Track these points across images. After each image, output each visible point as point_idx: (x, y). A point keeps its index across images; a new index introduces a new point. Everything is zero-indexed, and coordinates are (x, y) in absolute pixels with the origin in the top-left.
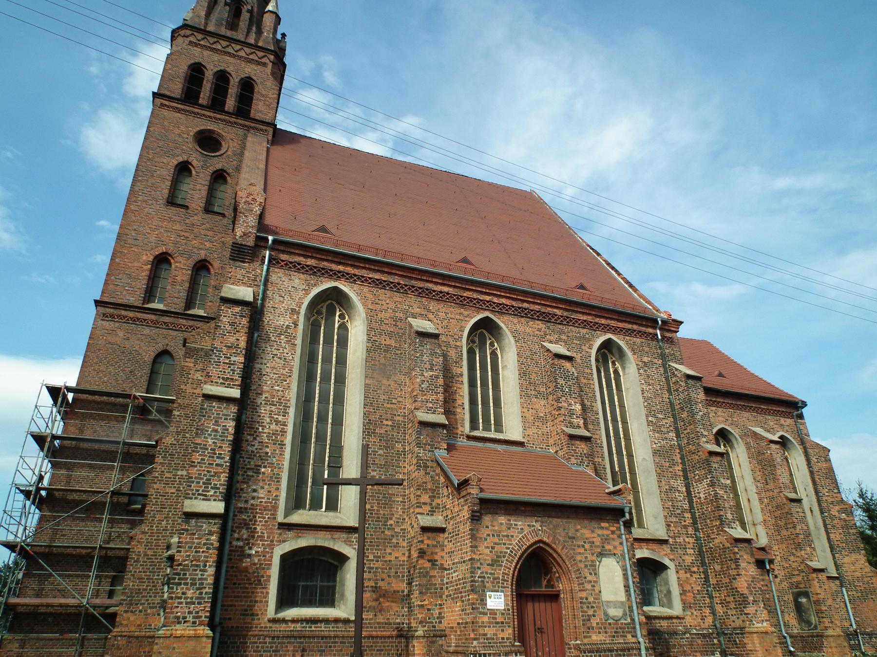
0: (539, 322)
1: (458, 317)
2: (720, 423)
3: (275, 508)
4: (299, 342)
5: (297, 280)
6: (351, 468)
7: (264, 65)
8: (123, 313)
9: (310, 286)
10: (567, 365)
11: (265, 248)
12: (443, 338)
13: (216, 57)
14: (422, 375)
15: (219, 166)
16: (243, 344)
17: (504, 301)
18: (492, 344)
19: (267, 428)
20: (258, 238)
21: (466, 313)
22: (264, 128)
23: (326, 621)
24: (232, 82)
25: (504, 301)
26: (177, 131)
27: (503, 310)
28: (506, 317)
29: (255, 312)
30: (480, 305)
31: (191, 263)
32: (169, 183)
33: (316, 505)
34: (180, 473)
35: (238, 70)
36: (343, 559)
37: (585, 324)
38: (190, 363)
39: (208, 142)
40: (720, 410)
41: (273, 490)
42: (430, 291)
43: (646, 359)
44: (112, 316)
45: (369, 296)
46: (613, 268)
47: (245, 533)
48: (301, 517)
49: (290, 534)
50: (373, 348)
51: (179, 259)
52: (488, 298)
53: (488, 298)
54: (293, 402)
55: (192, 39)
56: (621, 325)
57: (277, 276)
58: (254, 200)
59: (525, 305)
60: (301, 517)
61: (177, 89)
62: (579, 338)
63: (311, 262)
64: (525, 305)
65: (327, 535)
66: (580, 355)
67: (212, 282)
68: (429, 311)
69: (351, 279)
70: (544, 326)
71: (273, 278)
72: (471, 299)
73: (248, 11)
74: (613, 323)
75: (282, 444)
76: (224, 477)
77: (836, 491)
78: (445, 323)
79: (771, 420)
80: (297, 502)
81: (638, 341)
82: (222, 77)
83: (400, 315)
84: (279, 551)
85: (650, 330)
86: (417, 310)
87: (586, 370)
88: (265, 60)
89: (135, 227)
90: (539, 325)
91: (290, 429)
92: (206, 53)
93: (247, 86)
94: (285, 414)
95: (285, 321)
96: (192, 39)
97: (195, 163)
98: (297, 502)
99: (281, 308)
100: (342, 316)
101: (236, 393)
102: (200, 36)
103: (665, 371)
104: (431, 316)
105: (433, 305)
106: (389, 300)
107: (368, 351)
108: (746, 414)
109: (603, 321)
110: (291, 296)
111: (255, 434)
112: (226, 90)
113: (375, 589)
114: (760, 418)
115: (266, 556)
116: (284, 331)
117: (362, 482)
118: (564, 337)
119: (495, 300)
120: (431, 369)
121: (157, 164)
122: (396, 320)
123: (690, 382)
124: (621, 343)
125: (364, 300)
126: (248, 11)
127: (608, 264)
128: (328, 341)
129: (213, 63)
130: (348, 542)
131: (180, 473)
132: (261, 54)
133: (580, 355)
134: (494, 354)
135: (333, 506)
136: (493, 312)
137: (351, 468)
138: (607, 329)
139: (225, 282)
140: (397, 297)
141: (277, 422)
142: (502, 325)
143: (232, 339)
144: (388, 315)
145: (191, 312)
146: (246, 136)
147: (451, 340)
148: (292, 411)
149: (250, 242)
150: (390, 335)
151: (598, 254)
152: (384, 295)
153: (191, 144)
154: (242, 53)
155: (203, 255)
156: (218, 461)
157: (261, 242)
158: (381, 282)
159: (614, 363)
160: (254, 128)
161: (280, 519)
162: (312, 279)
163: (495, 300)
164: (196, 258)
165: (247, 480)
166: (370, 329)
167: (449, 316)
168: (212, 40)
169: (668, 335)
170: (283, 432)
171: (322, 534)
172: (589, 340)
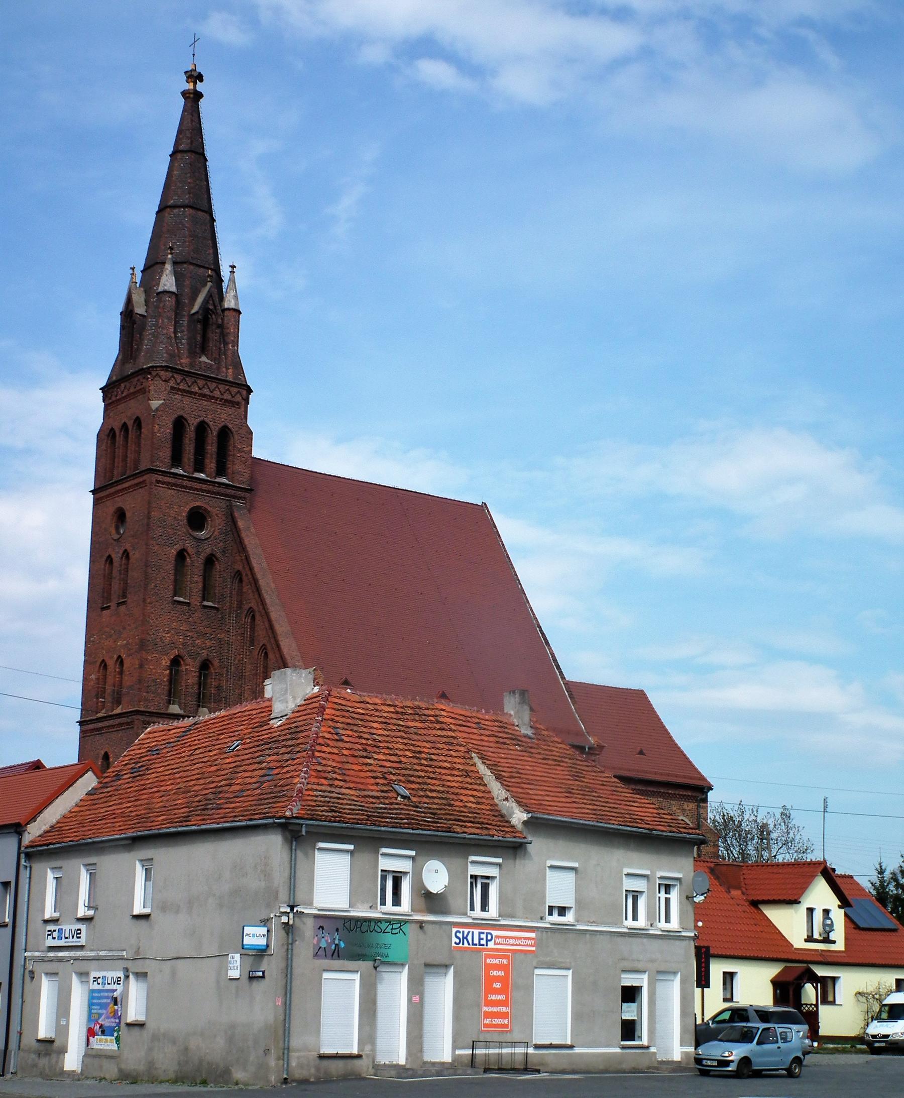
15: (208, 551)
31: (197, 663)
32: (172, 577)
51: (189, 661)
55: (172, 383)
82: (202, 428)
92: (187, 400)
93: (224, 434)
96: (172, 383)
97: (190, 550)
102: (179, 378)
154: (217, 394)
155: (204, 654)
160: (235, 497)
169: (593, 758)
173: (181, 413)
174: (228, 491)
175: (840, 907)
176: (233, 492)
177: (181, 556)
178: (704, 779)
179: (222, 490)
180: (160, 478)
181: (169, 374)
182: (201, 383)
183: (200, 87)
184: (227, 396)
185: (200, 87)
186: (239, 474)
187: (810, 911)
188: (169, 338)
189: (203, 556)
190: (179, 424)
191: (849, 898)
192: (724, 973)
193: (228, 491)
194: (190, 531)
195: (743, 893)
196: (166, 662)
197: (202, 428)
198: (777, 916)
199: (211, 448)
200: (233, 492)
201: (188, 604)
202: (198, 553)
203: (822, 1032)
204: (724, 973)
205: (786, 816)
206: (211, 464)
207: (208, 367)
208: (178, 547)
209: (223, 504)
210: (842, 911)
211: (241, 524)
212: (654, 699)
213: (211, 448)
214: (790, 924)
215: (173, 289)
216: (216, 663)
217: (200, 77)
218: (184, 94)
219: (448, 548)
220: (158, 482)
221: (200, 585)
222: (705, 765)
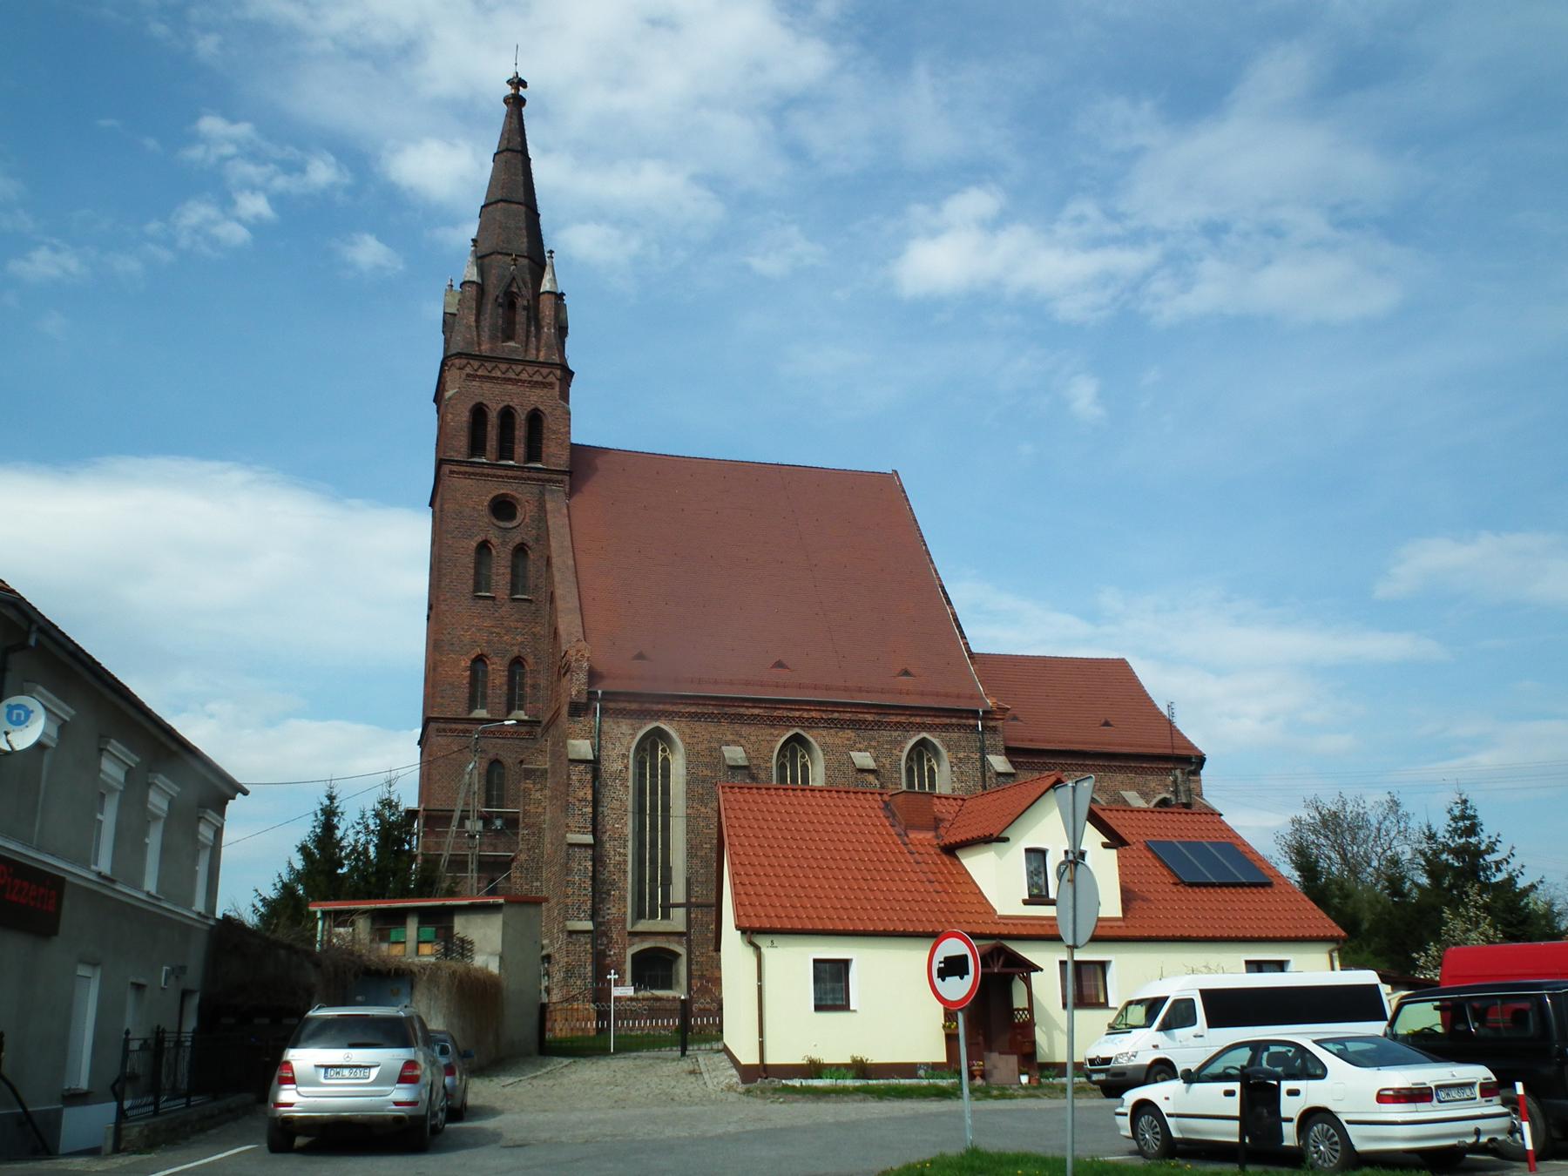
3: (625, 920)
4: (630, 784)
5: (624, 727)
6: (678, 893)
7: (551, 385)
8: (454, 726)
9: (636, 730)
10: (871, 778)
11: (596, 699)
13: (498, 389)
15: (518, 540)
16: (590, 797)
17: (813, 714)
18: (803, 757)
19: (613, 860)
20: (589, 693)
22: (560, 477)
23: (668, 1000)
24: (518, 421)
25: (813, 714)
27: (812, 724)
28: (815, 732)
29: (594, 765)
30: (788, 722)
31: (506, 661)
32: (472, 572)
33: (653, 916)
35: (524, 400)
36: (677, 955)
37: (898, 725)
38: (529, 784)
39: (503, 508)
41: (622, 906)
42: (742, 715)
43: (961, 755)
45: (687, 731)
46: (959, 626)
47: (605, 940)
48: (644, 925)
49: (636, 939)
50: (692, 781)
51: (496, 659)
52: (797, 714)
53: (797, 714)
54: (630, 836)
55: (468, 370)
56: (937, 721)
57: (609, 725)
59: (836, 715)
60: (644, 925)
61: (462, 443)
63: (634, 706)
64: (836, 715)
67: (529, 681)
71: (605, 727)
72: (781, 718)
73: (525, 308)
74: (928, 720)
75: (625, 872)
76: (589, 903)
79: (1153, 782)
80: (639, 915)
81: (955, 735)
82: (507, 414)
83: (715, 745)
84: (630, 952)
85: (972, 722)
86: (730, 737)
88: (551, 379)
90: (850, 734)
91: (630, 859)
92: (487, 385)
93: (535, 418)
94: (625, 847)
95: (618, 766)
96: (468, 370)
97: (494, 540)
98: (639, 915)
99: (614, 754)
100: (664, 750)
101: (589, 839)
102: (476, 364)
103: (983, 766)
104: (743, 741)
105: (745, 730)
106: (704, 730)
107: (688, 783)
108: (1120, 777)
109: (918, 720)
110: (624, 739)
111: (604, 866)
112: (513, 429)
113: (702, 977)
114: (1139, 779)
115: (622, 954)
116: (619, 775)
117: (688, 905)
119: (805, 715)
122: (711, 750)
123: (1002, 779)
124: (935, 741)
125: (682, 734)
126: (525, 308)
127: (956, 620)
128: (654, 776)
129: (495, 397)
130: (680, 943)
132: (545, 371)
134: (805, 767)
135: (666, 916)
136: (802, 727)
137: (678, 893)
139: (567, 737)
143: (581, 794)
146: (542, 494)
148: (630, 844)
149: (584, 700)
150: (707, 765)
151: (949, 602)
153: (486, 518)
154: (524, 376)
155: (516, 651)
157: (592, 696)
158: (696, 714)
159: (929, 760)
160: (549, 481)
161: (629, 928)
162: (636, 723)
163: (805, 715)
164: (509, 657)
165: (602, 901)
166: (689, 762)
168: (489, 365)
169: (992, 724)
170: (625, 862)
173: (480, 399)
174: (541, 476)
175: (1105, 846)
176: (547, 476)
177: (484, 547)
178: (1192, 747)
179: (535, 475)
180: (455, 468)
181: (464, 361)
182: (503, 367)
183: (522, 91)
184: (537, 378)
185: (522, 91)
186: (555, 456)
187: (1036, 855)
188: (469, 327)
189: (510, 547)
190: (479, 412)
191: (1122, 831)
192: (816, 961)
193: (541, 476)
194: (502, 524)
195: (937, 837)
196: (465, 662)
197: (507, 414)
198: (982, 866)
199: (520, 433)
200: (547, 476)
201: (493, 598)
202: (504, 543)
203: (941, 1056)
204: (816, 961)
205: (1394, 805)
206: (520, 449)
207: (515, 350)
208: (479, 539)
209: (536, 490)
210: (1113, 853)
211: (548, 506)
212: (1149, 676)
213: (520, 433)
214: (998, 878)
215: (475, 278)
216: (530, 659)
217: (523, 83)
218: (506, 100)
219: (859, 527)
220: (452, 472)
221: (508, 577)
222: (1196, 735)
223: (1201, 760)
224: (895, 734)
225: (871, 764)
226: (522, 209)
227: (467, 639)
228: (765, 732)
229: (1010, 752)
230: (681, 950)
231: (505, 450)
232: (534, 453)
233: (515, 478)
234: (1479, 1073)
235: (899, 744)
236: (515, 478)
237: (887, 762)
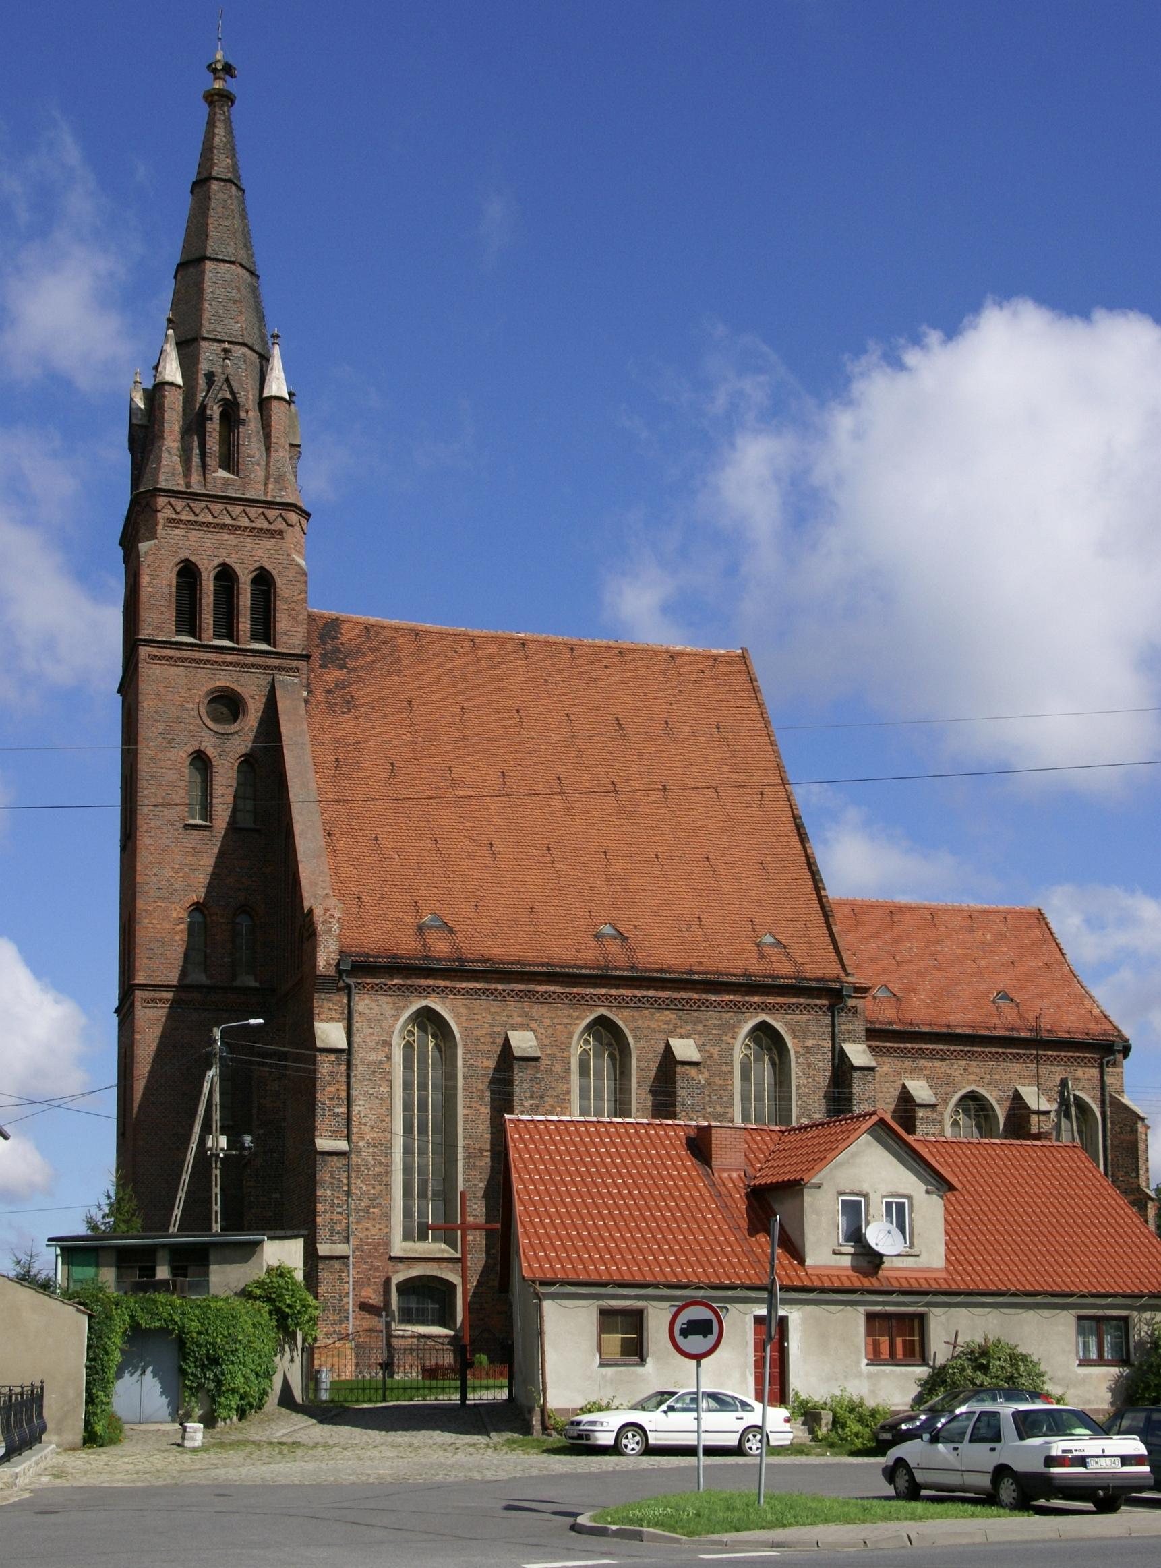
0: (667, 1012)
1: (566, 1021)
2: (970, 1083)
12: (545, 1062)
14: (522, 1105)
21: (576, 1014)
22: (294, 664)
26: (178, 700)
28: (626, 1012)
34: (274, 1196)
35: (246, 557)
37: (729, 1006)
39: (227, 704)
40: (974, 1064)
43: (809, 1043)
44: (153, 1000)
45: (463, 1011)
49: (401, 1266)
58: (332, 916)
62: (720, 1027)
65: (433, 1265)
66: (718, 1048)
68: (532, 1018)
69: (441, 992)
70: (673, 1016)
77: (1134, 1175)
78: (550, 1032)
82: (226, 575)
87: (724, 1068)
89: (155, 871)
90: (670, 1015)
93: (264, 581)
104: (533, 1025)
105: (537, 1011)
108: (1018, 1067)
118: (700, 1028)
120: (532, 1097)
121: (162, 764)
124: (778, 1026)
125: (457, 1016)
130: (453, 1271)
131: (274, 1196)
133: (718, 1048)
138: (763, 1007)
140: (495, 1006)
141: (381, 1163)
142: (620, 1023)
144: (484, 1032)
145: (237, 983)
147: (556, 1050)
152: (479, 1005)
156: (340, 1210)
160: (280, 669)
167: (556, 1021)
171: (430, 1264)
172: (734, 1026)
176: (277, 662)
180: (155, 651)
186: (291, 632)
199: (245, 599)
202: (223, 754)
206: (244, 625)
213: (245, 599)
220: (154, 657)
223: (1126, 1050)
224: (725, 1015)
225: (695, 1056)
226: (703, 1361)
227: (178, 884)
228: (562, 1014)
229: (872, 1034)
230: (455, 1279)
231: (227, 627)
232: (265, 628)
233: (236, 664)
234: (825, 1002)
235: (733, 1029)
236: (236, 664)
237: (715, 1051)
